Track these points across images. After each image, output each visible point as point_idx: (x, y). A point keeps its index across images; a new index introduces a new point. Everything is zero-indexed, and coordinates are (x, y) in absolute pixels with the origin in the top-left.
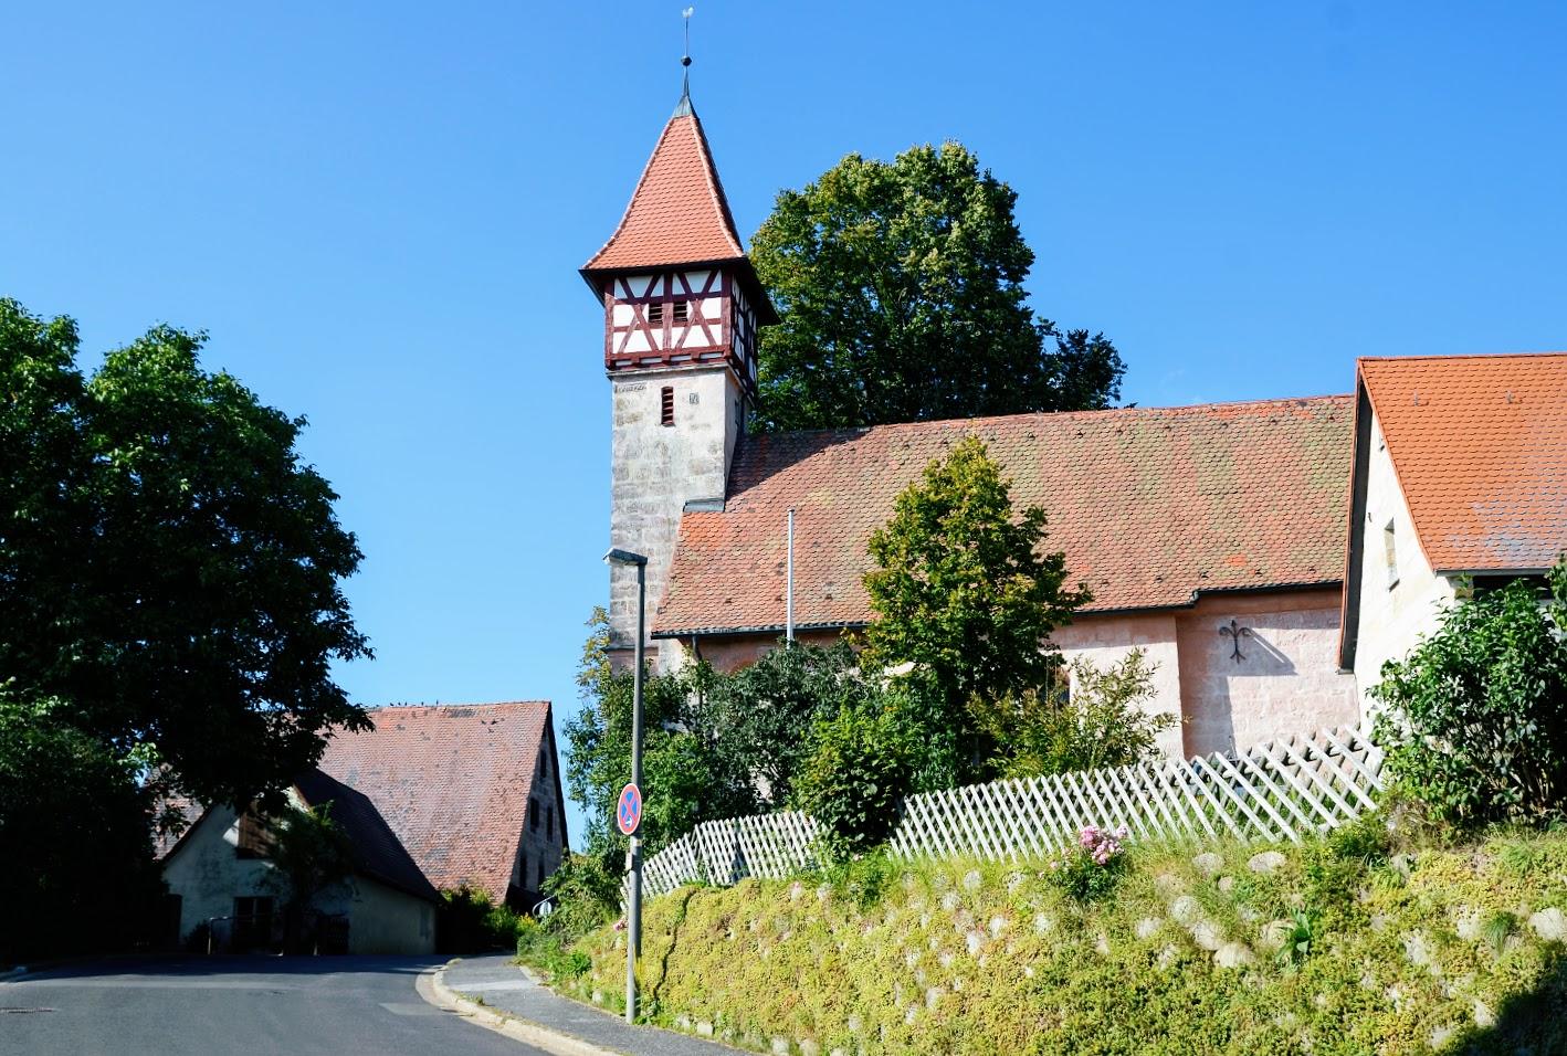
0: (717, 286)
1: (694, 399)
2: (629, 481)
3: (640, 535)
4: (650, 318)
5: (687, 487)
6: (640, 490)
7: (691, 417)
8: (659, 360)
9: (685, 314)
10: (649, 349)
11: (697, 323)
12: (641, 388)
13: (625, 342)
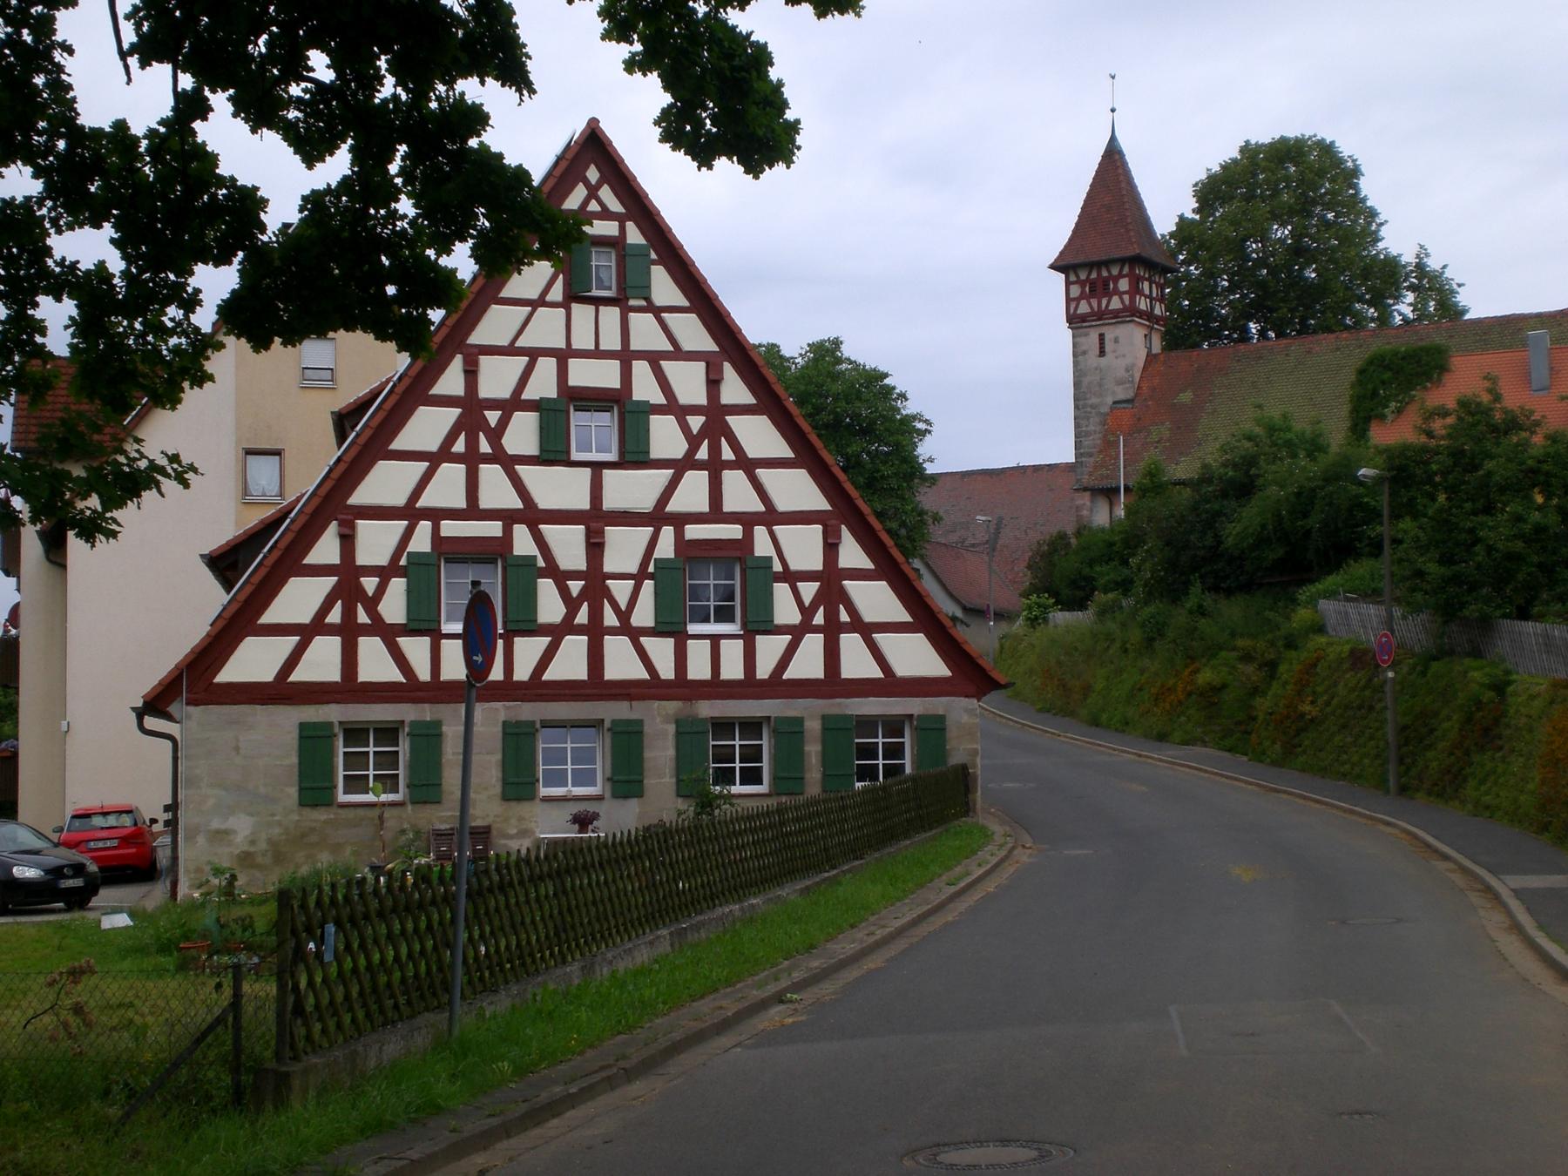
0: (1126, 270)
1: (1116, 340)
5: (1114, 393)
12: (1086, 335)
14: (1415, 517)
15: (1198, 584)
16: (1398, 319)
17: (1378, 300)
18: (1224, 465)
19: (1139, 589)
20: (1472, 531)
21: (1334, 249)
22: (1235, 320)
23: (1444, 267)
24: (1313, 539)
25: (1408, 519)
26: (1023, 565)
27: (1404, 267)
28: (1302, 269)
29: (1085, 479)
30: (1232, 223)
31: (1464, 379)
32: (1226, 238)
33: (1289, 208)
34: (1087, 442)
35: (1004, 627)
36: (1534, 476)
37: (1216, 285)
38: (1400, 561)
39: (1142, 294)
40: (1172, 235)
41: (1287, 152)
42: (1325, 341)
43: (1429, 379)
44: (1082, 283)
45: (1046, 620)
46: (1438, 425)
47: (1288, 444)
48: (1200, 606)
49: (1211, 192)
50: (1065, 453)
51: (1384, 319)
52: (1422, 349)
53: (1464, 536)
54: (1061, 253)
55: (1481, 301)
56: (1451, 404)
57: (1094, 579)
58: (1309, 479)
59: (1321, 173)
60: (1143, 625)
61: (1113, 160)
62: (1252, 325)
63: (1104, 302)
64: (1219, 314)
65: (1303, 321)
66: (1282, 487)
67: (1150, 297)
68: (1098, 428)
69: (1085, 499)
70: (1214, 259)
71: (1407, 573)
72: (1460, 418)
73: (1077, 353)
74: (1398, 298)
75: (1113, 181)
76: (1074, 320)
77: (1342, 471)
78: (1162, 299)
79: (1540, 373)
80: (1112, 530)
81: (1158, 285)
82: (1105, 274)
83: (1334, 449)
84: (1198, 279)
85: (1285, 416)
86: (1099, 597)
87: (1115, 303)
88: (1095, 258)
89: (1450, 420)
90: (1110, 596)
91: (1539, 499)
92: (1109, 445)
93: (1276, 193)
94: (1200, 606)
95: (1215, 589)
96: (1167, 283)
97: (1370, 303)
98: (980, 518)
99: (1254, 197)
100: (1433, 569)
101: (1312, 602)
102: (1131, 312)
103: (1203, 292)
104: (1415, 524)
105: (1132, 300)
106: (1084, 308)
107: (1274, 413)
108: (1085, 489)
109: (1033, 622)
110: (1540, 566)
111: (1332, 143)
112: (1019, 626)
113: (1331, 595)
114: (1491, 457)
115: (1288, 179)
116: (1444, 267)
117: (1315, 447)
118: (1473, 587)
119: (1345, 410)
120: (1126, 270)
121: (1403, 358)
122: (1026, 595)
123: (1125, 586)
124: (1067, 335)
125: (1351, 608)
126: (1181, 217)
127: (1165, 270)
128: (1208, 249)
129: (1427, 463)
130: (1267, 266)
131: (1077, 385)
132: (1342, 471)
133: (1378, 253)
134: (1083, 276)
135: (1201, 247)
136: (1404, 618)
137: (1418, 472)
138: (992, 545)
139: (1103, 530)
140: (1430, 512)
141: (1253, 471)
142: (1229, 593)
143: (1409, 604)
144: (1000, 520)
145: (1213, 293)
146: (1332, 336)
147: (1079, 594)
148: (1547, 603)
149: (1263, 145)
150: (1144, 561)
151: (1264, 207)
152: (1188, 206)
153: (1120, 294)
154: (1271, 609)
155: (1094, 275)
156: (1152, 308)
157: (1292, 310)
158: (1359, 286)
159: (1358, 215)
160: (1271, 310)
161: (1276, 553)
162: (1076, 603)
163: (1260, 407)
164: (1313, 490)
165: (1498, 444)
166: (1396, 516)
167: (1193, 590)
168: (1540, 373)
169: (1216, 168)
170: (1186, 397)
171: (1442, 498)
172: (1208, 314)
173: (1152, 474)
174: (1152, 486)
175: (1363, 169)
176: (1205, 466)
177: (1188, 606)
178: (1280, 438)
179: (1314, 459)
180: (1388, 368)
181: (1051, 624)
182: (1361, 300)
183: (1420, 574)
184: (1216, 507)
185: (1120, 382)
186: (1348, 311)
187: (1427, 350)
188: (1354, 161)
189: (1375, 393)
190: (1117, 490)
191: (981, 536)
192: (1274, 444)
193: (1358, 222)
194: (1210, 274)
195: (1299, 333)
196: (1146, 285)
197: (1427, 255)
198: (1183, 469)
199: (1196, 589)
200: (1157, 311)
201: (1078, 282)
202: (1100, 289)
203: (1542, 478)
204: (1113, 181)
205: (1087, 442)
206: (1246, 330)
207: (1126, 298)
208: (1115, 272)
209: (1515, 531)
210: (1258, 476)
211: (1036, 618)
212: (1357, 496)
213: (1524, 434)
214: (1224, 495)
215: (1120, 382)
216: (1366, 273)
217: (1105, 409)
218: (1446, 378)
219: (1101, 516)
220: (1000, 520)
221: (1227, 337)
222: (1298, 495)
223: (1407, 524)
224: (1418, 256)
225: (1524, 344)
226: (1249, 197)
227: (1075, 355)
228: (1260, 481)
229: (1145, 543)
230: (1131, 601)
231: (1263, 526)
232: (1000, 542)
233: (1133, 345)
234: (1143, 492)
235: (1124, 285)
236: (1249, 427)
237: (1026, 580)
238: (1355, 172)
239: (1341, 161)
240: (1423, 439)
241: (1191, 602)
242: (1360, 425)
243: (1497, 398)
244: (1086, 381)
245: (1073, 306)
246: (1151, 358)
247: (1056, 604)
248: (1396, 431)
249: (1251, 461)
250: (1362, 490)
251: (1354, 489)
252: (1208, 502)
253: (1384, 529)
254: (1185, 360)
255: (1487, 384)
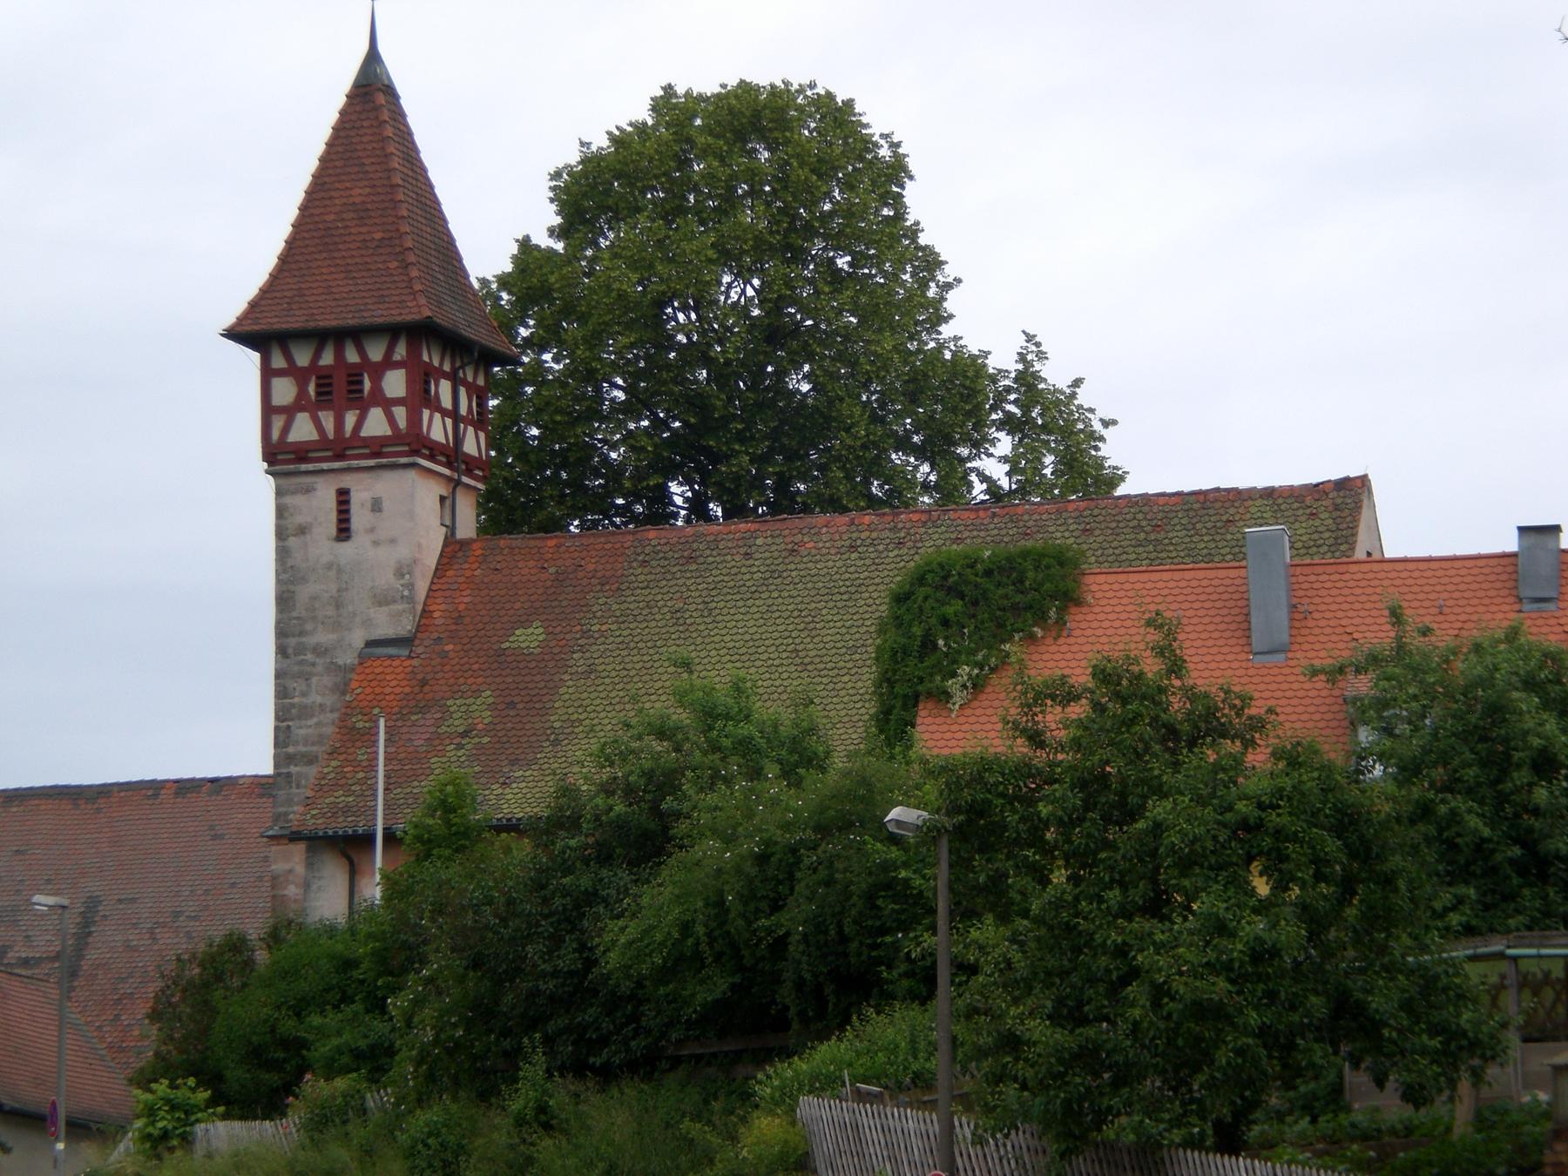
0: (401, 352)
1: (376, 506)
2: (294, 614)
3: (309, 686)
4: (318, 394)
5: (367, 623)
6: (309, 627)
7: (372, 530)
8: (366, 451)
9: (361, 391)
10: (389, 433)
11: (376, 404)
12: (308, 490)
13: (286, 430)
14: (1003, 918)
15: (539, 1058)
16: (979, 488)
17: (938, 448)
18: (607, 789)
19: (405, 1068)
20: (1121, 952)
21: (848, 335)
22: (638, 476)
23: (1077, 383)
24: (792, 966)
25: (989, 919)
26: (143, 1009)
27: (993, 379)
28: (781, 374)
29: (306, 809)
30: (633, 265)
31: (1109, 625)
32: (622, 296)
33: (755, 209)
34: (302, 730)
35: (89, 1153)
36: (1251, 837)
37: (599, 396)
38: (972, 1012)
39: (436, 406)
40: (504, 281)
41: (752, 115)
42: (827, 528)
43: (1041, 618)
44: (300, 375)
45: (187, 1140)
46: (1053, 719)
47: (745, 747)
48: (542, 1109)
49: (589, 193)
50: (248, 750)
51: (951, 488)
52: (1025, 554)
53: (1104, 961)
54: (254, 305)
55: (1149, 459)
56: (1081, 677)
57: (303, 1044)
58: (787, 826)
59: (824, 169)
60: (411, 1153)
61: (372, 104)
62: (674, 487)
63: (350, 419)
64: (605, 460)
65: (783, 484)
66: (729, 841)
67: (454, 414)
68: (329, 700)
69: (293, 860)
70: (595, 340)
71: (985, 1040)
72: (1098, 708)
73: (287, 531)
74: (980, 445)
75: (370, 156)
76: (280, 456)
77: (856, 812)
78: (480, 422)
79: (1270, 619)
80: (352, 931)
81: (472, 389)
82: (352, 356)
83: (839, 762)
84: (560, 382)
85: (738, 688)
86: (315, 1087)
87: (376, 424)
88: (351, 321)
89: (1079, 710)
90: (341, 1083)
91: (1262, 888)
92: (353, 736)
93: (730, 203)
94: (542, 1109)
95: (578, 1069)
96: (493, 386)
97: (922, 453)
98: (43, 900)
99: (681, 210)
100: (1038, 1030)
101: (786, 1101)
102: (410, 447)
103: (573, 409)
104: (1005, 931)
105: (414, 419)
106: (303, 430)
107: (717, 677)
108: (295, 837)
109: (158, 1144)
110: (1263, 1032)
111: (849, 104)
112: (125, 1150)
113: (824, 1084)
114: (1161, 792)
115: (753, 176)
116: (1077, 383)
117: (801, 757)
118: (1125, 1077)
119: (868, 676)
120: (401, 352)
121: (988, 573)
122: (144, 1080)
123: (374, 1061)
124: (261, 487)
125: (866, 1116)
126: (525, 244)
127: (488, 358)
128: (582, 319)
129: (1030, 801)
130: (707, 361)
131: (284, 600)
132: (856, 812)
133: (941, 347)
134: (303, 358)
135: (568, 311)
136: (979, 1141)
137: (1012, 819)
138: (69, 966)
139: (331, 930)
140: (1035, 907)
141: (668, 803)
142: (607, 1076)
143: (989, 1110)
144: (92, 904)
145: (593, 413)
146: (845, 519)
147: (273, 1078)
148: (1280, 1116)
149: (701, 98)
150: (418, 1003)
151: (703, 239)
152: (539, 221)
153: (387, 404)
154: (696, 1117)
155: (327, 359)
156: (458, 439)
157: (761, 460)
158: (900, 416)
159: (900, 264)
160: (716, 458)
161: (713, 987)
162: (263, 1102)
163: (687, 665)
164: (794, 851)
165: (1176, 765)
166: (964, 913)
167: (526, 1071)
168: (1270, 619)
169: (600, 142)
170: (529, 637)
171: (1059, 876)
172: (581, 458)
173: (446, 807)
174: (448, 832)
175: (912, 164)
176: (566, 791)
177: (515, 1106)
178: (727, 738)
179: (798, 784)
180: (955, 592)
181: (200, 1149)
182: (903, 444)
183: (1012, 1043)
184: (585, 882)
185: (382, 600)
186: (877, 466)
187: (1038, 558)
188: (895, 146)
189: (928, 645)
190: (369, 839)
191: (45, 943)
192: (715, 748)
193: (902, 278)
194: (588, 374)
195: (775, 509)
196: (445, 388)
197: (1041, 356)
198: (520, 796)
199: (533, 1069)
200: (470, 447)
201: (292, 371)
202: (341, 389)
203: (1267, 842)
204: (370, 156)
205: (302, 730)
206: (664, 497)
207: (400, 413)
208: (376, 353)
209: (1211, 955)
210: (678, 815)
211: (166, 1135)
212: (887, 866)
213: (1231, 747)
214: (604, 856)
215: (382, 600)
216: (915, 388)
217: (348, 658)
218: (1075, 618)
219: (328, 899)
220: (92, 904)
221: (621, 511)
222: (762, 859)
223: (986, 931)
224: (1022, 358)
225: (1238, 551)
226: (672, 211)
227: (281, 534)
228: (681, 828)
229: (424, 962)
230: (387, 1096)
231: (686, 928)
232: (92, 955)
233: (413, 518)
234: (427, 845)
235: (395, 383)
236: (660, 706)
237: (146, 1041)
238: (897, 170)
239: (868, 144)
240: (1022, 747)
241: (520, 1101)
242: (894, 722)
243: (1176, 667)
244: (303, 593)
245: (278, 423)
246: (453, 548)
247: (212, 1102)
248: (966, 731)
249: (663, 782)
250: (895, 853)
251: (880, 851)
252: (568, 871)
253: (938, 942)
254: (524, 554)
255: (1154, 636)
